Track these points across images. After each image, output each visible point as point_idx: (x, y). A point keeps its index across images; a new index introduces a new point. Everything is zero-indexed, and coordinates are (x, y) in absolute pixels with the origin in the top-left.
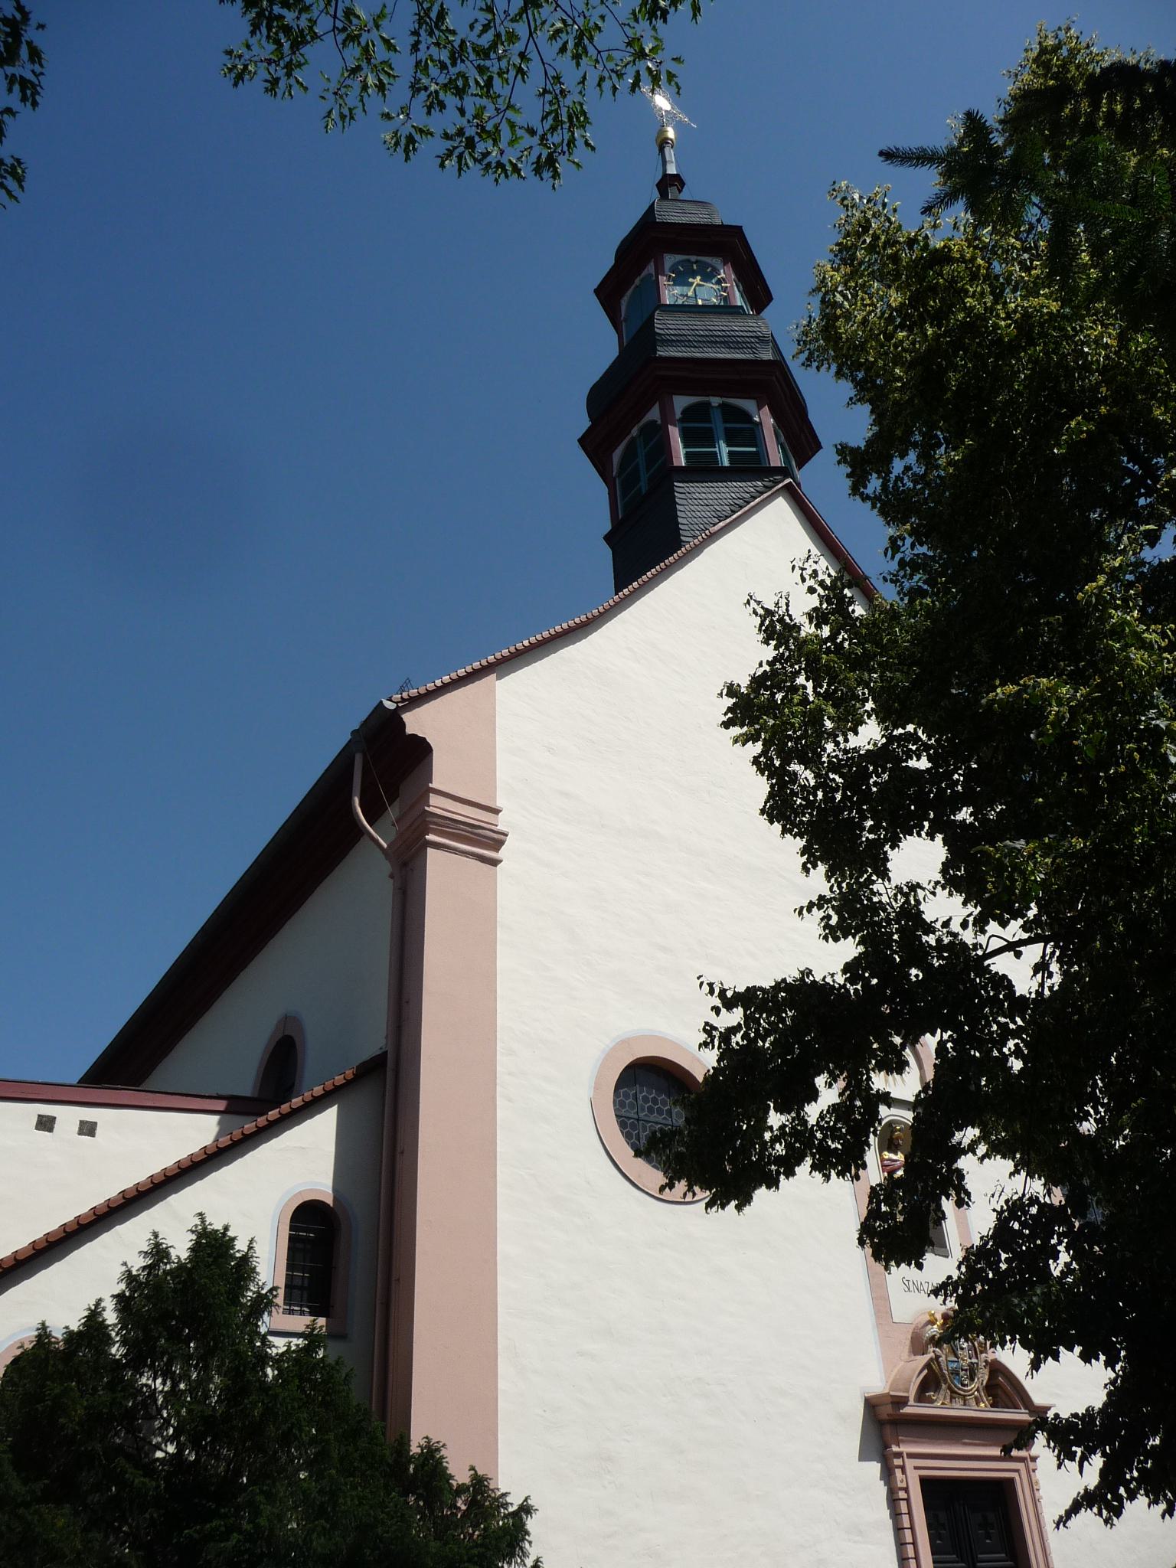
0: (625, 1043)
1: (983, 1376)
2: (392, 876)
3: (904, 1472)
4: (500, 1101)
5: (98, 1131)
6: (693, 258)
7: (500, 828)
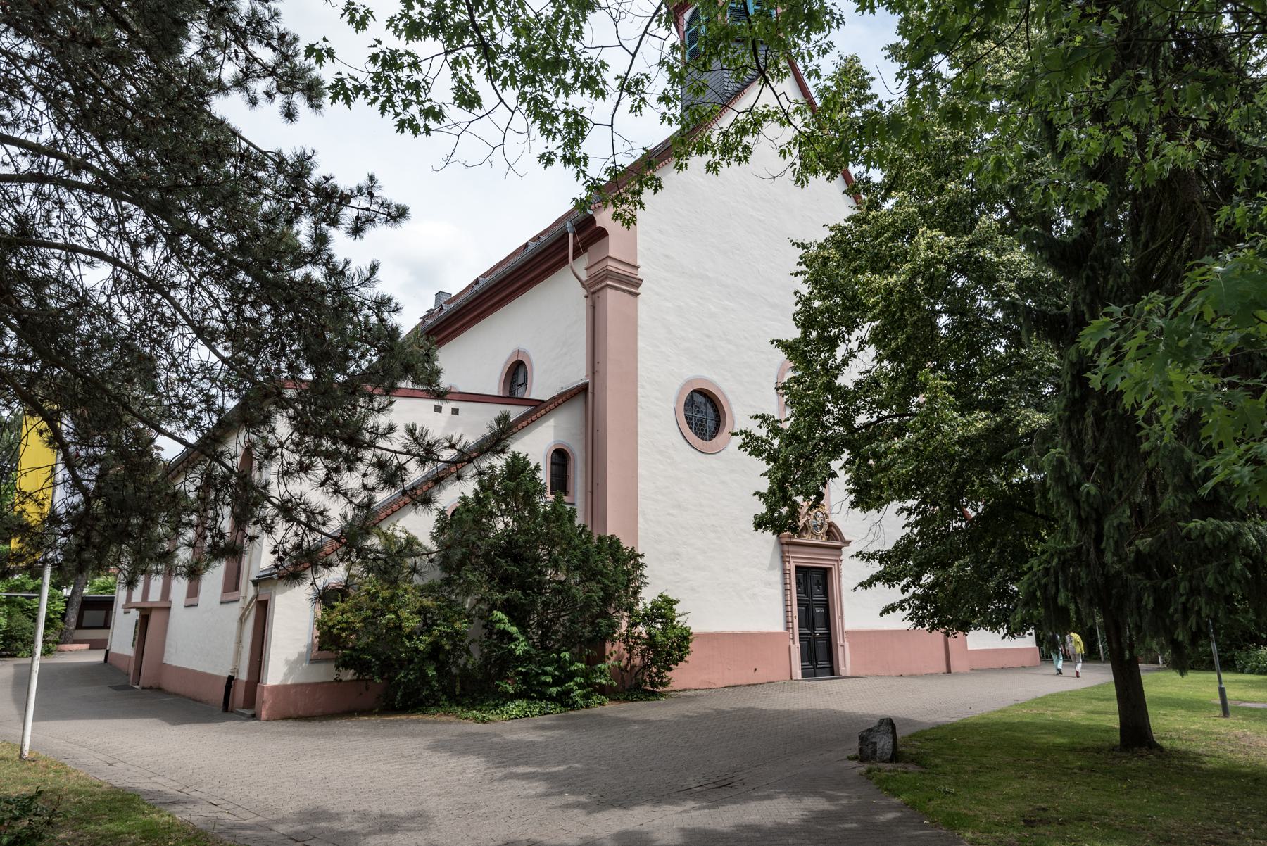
0: (689, 382)
1: (826, 528)
2: (586, 297)
4: (639, 409)
7: (639, 277)
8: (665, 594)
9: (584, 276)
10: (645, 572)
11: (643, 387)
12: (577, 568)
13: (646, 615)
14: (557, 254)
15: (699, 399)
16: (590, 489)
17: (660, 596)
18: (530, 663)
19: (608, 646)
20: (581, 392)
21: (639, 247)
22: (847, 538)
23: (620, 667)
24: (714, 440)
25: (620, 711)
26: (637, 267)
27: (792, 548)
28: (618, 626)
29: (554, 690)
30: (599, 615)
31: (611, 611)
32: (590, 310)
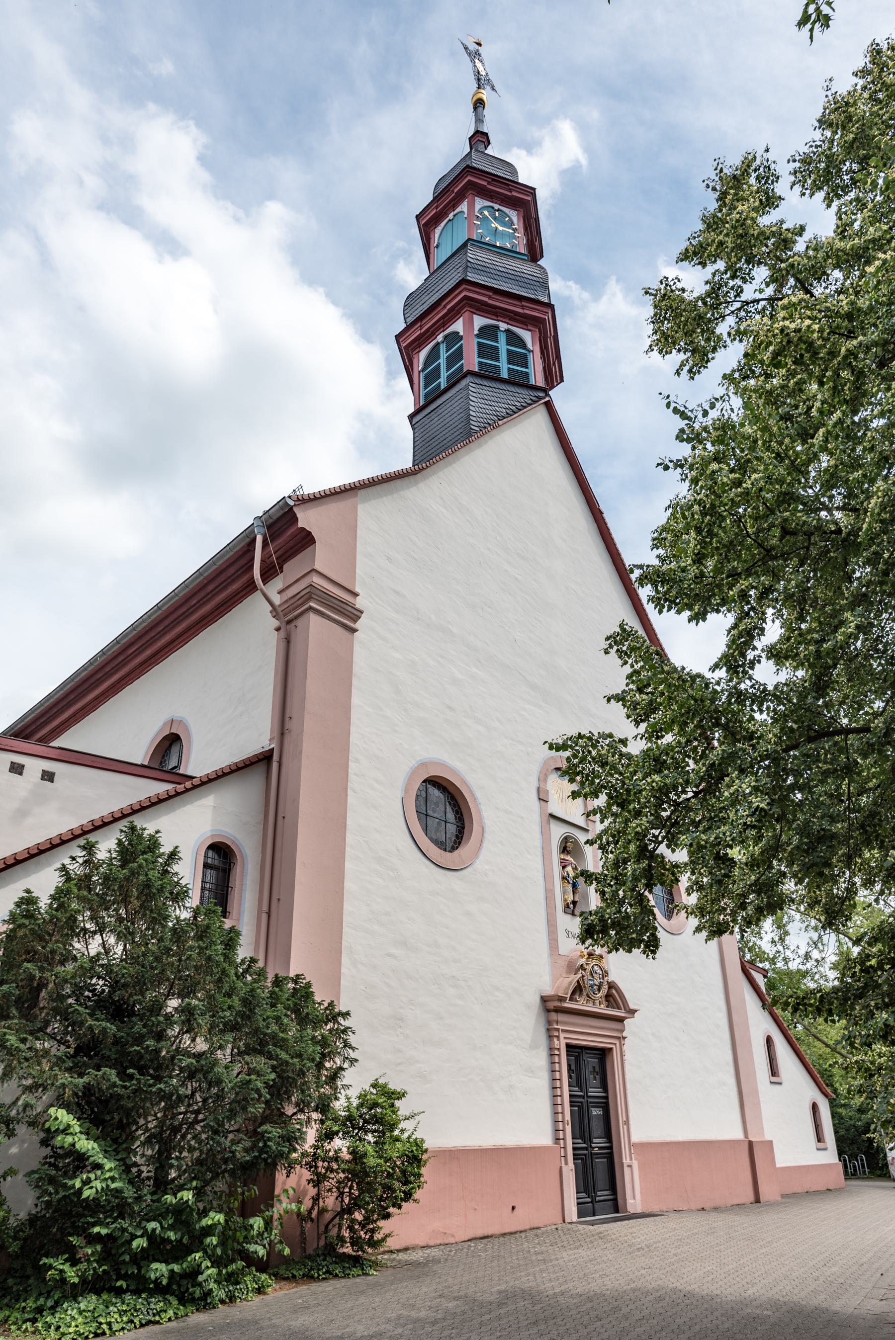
0: (423, 765)
2: (278, 629)
3: (559, 1040)
4: (350, 792)
5: (55, 779)
6: (497, 206)
7: (357, 606)
8: (381, 1081)
9: (277, 600)
10: (352, 1039)
11: (357, 761)
12: (232, 1027)
13: (350, 1118)
14: (239, 577)
15: (435, 792)
16: (265, 908)
17: (374, 1086)
18: (122, 1216)
19: (280, 1176)
20: (265, 759)
21: (358, 571)
22: (632, 1006)
23: (299, 1214)
24: (456, 852)
25: (297, 1310)
26: (356, 595)
27: (562, 1017)
28: (300, 1137)
29: (159, 1270)
30: (265, 1119)
31: (290, 1110)
32: (283, 645)
